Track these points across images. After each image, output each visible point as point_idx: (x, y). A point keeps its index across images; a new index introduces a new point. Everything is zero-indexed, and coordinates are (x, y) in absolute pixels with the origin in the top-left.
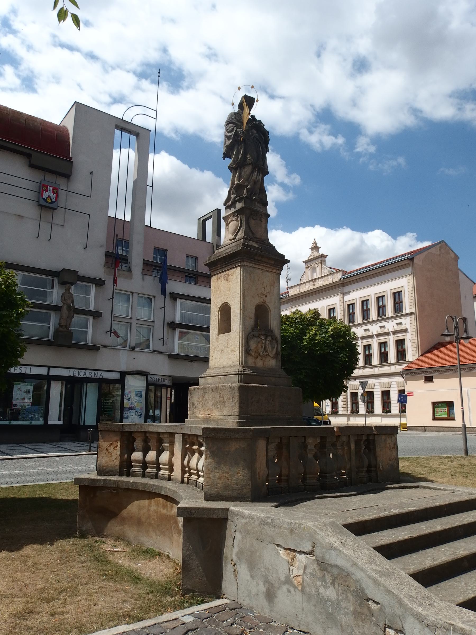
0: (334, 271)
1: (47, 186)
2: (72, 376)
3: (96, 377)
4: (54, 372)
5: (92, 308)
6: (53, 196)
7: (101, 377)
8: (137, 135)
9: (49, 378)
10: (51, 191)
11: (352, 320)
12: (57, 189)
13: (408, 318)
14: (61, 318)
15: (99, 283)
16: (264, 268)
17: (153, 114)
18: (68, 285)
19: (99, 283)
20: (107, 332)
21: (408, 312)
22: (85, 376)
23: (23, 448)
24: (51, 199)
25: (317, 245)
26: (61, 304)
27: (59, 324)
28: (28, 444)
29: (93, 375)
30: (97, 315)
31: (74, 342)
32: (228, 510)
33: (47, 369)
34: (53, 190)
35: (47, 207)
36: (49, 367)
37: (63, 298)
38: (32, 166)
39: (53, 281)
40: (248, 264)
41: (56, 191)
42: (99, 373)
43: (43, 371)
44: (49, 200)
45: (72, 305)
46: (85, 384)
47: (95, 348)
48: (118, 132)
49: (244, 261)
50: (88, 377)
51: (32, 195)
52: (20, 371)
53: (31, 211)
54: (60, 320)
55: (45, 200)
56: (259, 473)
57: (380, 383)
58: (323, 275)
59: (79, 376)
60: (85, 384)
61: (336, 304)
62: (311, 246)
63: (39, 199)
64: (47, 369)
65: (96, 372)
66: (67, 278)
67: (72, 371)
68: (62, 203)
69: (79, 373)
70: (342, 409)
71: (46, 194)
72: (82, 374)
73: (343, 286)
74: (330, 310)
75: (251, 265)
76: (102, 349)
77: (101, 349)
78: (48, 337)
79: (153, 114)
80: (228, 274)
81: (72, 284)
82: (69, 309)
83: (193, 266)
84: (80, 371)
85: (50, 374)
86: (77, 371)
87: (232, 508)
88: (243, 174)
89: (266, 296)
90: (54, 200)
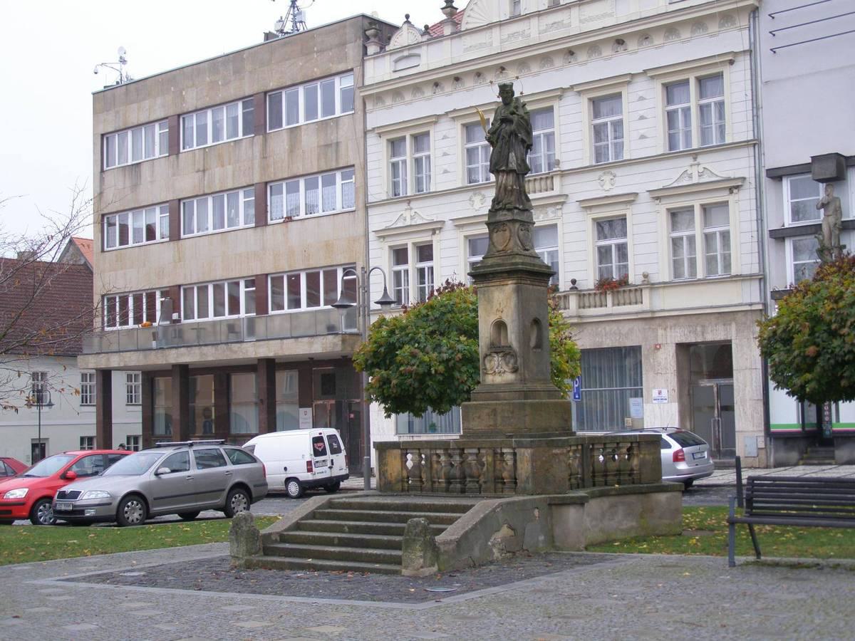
40: (482, 286)
75: (485, 285)
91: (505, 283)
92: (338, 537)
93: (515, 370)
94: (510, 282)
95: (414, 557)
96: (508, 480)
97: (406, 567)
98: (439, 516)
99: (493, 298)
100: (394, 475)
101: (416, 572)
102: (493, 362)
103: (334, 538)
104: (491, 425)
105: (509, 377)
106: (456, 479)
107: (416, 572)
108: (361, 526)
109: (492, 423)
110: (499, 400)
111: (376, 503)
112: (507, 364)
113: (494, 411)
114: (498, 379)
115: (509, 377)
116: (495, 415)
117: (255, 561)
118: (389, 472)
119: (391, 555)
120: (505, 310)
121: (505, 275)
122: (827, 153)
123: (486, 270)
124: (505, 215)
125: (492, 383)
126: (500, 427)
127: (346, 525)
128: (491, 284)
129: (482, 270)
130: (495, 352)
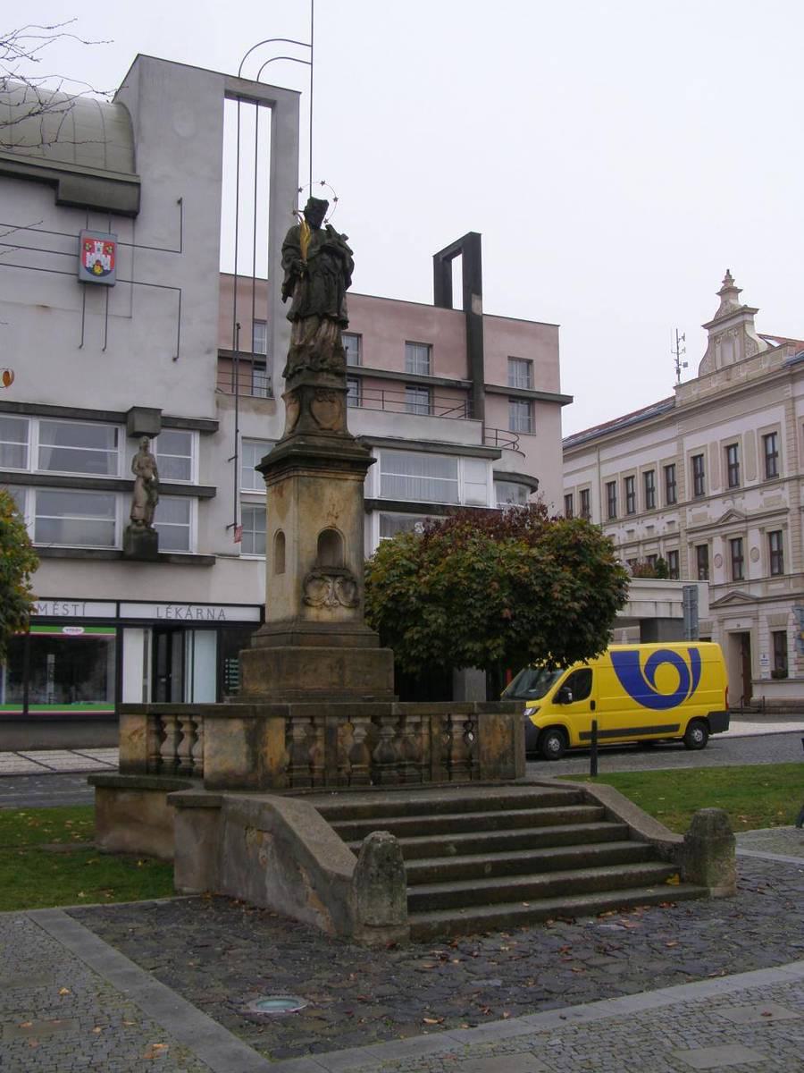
0: (776, 344)
1: (91, 242)
2: (164, 617)
3: (210, 619)
4: (128, 612)
5: (195, 481)
6: (106, 261)
7: (222, 619)
8: (271, 104)
9: (121, 624)
10: (101, 249)
11: (772, 472)
12: (113, 245)
13: (787, 485)
14: (135, 504)
15: (208, 429)
16: (332, 476)
17: (304, 53)
18: (144, 439)
19: (208, 429)
20: (228, 527)
21: (786, 476)
22: (189, 618)
23: (76, 756)
24: (102, 267)
25: (735, 285)
26: (133, 477)
27: (131, 517)
28: (87, 750)
29: (205, 614)
30: (205, 495)
31: (161, 551)
32: (221, 798)
33: (114, 606)
34: (104, 247)
35: (93, 286)
36: (118, 602)
37: (138, 467)
38: (62, 204)
39: (116, 430)
40: (306, 474)
41: (110, 249)
42: (218, 610)
43: (108, 611)
44: (98, 270)
45: (153, 477)
46: (191, 632)
47: (203, 563)
48: (230, 105)
49: (298, 470)
50: (195, 618)
51: (66, 264)
52: (65, 612)
53: (64, 296)
54: (133, 509)
55: (91, 271)
56: (271, 759)
57: (627, 632)
58: (748, 357)
59: (179, 618)
60: (191, 632)
61: (779, 423)
62: (720, 286)
63: (78, 269)
64: (114, 606)
65: (211, 608)
66: (138, 424)
67: (163, 608)
68: (123, 272)
69: (177, 613)
70: (796, 668)
71: (91, 259)
72: (183, 614)
73: (793, 382)
74: (766, 437)
75: (312, 474)
76: (220, 563)
77: (217, 560)
78: (113, 543)
79: (304, 53)
80: (282, 487)
81: (152, 436)
82: (150, 488)
83: (424, 365)
84: (179, 607)
85: (122, 616)
86: (173, 607)
87: (225, 795)
88: (306, 328)
89: (336, 517)
90: (107, 268)
91: (346, 476)
92: (492, 862)
93: (354, 604)
94: (353, 477)
95: (726, 866)
96: (458, 761)
97: (714, 884)
98: (565, 812)
99: (323, 495)
100: (277, 759)
101: (729, 888)
102: (324, 590)
103: (485, 863)
104: (334, 683)
105: (345, 613)
106: (393, 762)
107: (729, 888)
108: (480, 840)
109: (336, 680)
110: (338, 646)
111: (428, 803)
112: (346, 594)
113: (341, 663)
114: (326, 615)
115: (345, 613)
116: (340, 668)
117: (436, 926)
118: (269, 757)
119: (641, 873)
120: (341, 516)
121: (346, 466)
122: (626, 414)
123: (305, 451)
124: (333, 380)
125: (315, 620)
126: (350, 686)
127: (451, 842)
128: (320, 475)
129: (334, 453)
130: (330, 576)
